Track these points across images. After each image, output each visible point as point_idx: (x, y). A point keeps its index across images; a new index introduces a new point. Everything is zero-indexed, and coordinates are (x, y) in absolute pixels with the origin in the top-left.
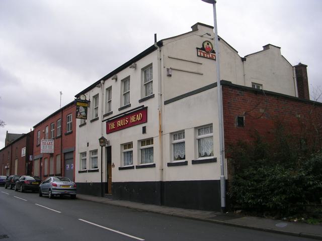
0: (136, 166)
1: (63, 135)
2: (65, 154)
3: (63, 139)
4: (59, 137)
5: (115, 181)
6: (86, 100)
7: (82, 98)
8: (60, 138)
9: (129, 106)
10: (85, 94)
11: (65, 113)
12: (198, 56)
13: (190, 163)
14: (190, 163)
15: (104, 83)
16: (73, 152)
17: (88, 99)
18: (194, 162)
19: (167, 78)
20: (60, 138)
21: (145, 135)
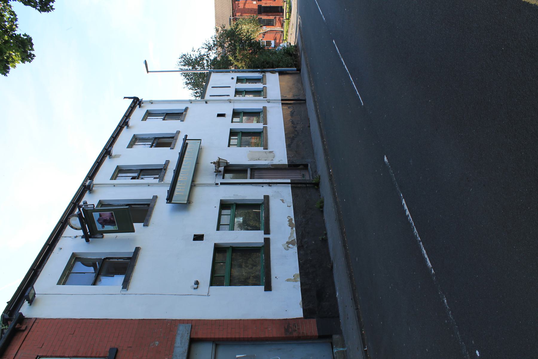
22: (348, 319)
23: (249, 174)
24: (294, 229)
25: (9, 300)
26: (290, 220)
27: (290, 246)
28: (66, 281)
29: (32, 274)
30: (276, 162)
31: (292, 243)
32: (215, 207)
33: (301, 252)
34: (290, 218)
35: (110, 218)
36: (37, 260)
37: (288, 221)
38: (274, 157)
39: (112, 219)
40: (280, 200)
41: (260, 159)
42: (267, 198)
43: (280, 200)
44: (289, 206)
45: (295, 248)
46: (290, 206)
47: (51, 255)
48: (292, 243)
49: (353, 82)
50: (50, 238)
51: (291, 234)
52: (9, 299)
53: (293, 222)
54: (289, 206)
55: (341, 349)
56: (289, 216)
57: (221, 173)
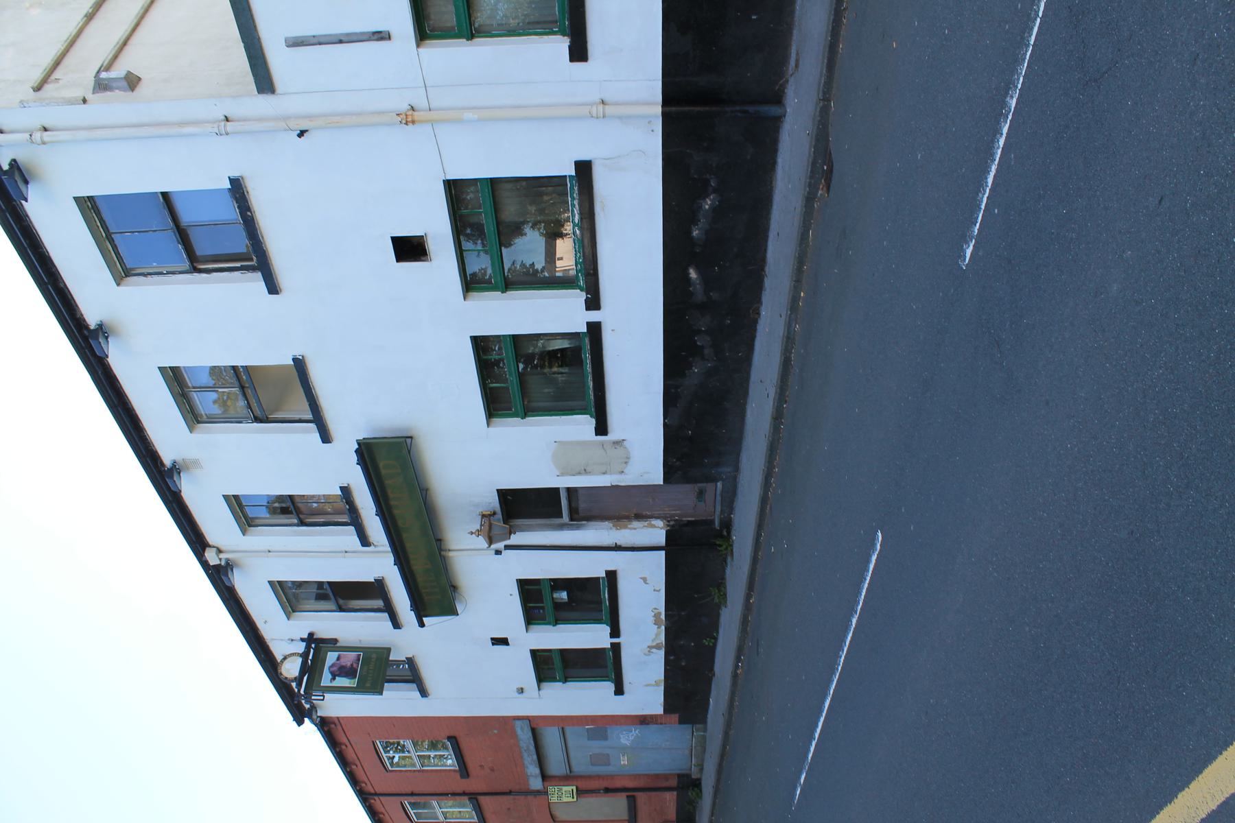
0: (588, 308)
1: (472, 785)
2: (544, 777)
3: (484, 788)
4: (479, 809)
5: (660, 698)
6: (305, 655)
7: (291, 669)
8: (482, 799)
9: (346, 491)
10: (279, 658)
11: (376, 781)
12: (323, 700)
13: (594, 316)
14: (594, 316)
15: (219, 551)
16: (535, 726)
17: (301, 647)
18: (593, 303)
19: (142, 89)
20: (482, 799)
21: (431, 246)
22: (781, 316)
23: (565, 499)
24: (663, 628)
25: (292, 719)
26: (657, 616)
27: (654, 650)
28: (107, 228)
29: (60, 304)
30: (631, 477)
31: (658, 647)
32: (511, 595)
33: (668, 668)
34: (656, 611)
35: (352, 665)
36: (105, 396)
37: (653, 616)
38: (626, 463)
39: (355, 665)
40: (641, 578)
41: (589, 469)
42: (612, 576)
43: (641, 578)
44: (657, 591)
45: (662, 653)
46: (659, 591)
47: (67, 283)
48: (658, 647)
49: (814, 743)
50: (106, 398)
51: (657, 635)
52: (291, 718)
53: (663, 617)
54: (657, 591)
55: (702, 733)
56: (655, 609)
57: (496, 517)
